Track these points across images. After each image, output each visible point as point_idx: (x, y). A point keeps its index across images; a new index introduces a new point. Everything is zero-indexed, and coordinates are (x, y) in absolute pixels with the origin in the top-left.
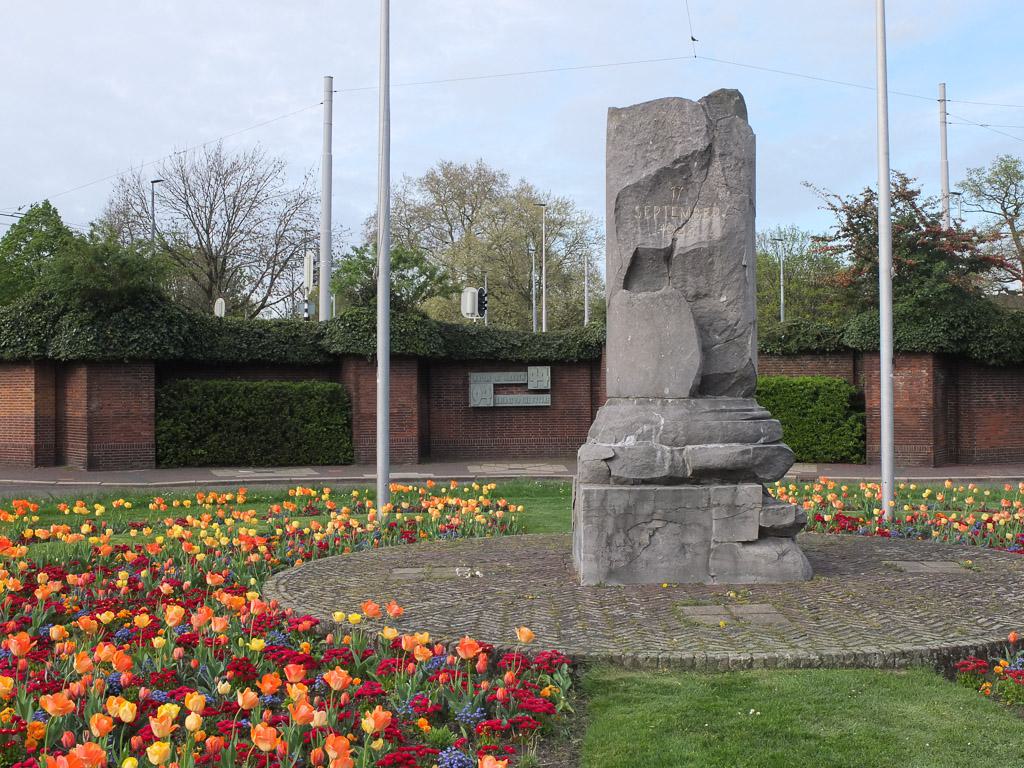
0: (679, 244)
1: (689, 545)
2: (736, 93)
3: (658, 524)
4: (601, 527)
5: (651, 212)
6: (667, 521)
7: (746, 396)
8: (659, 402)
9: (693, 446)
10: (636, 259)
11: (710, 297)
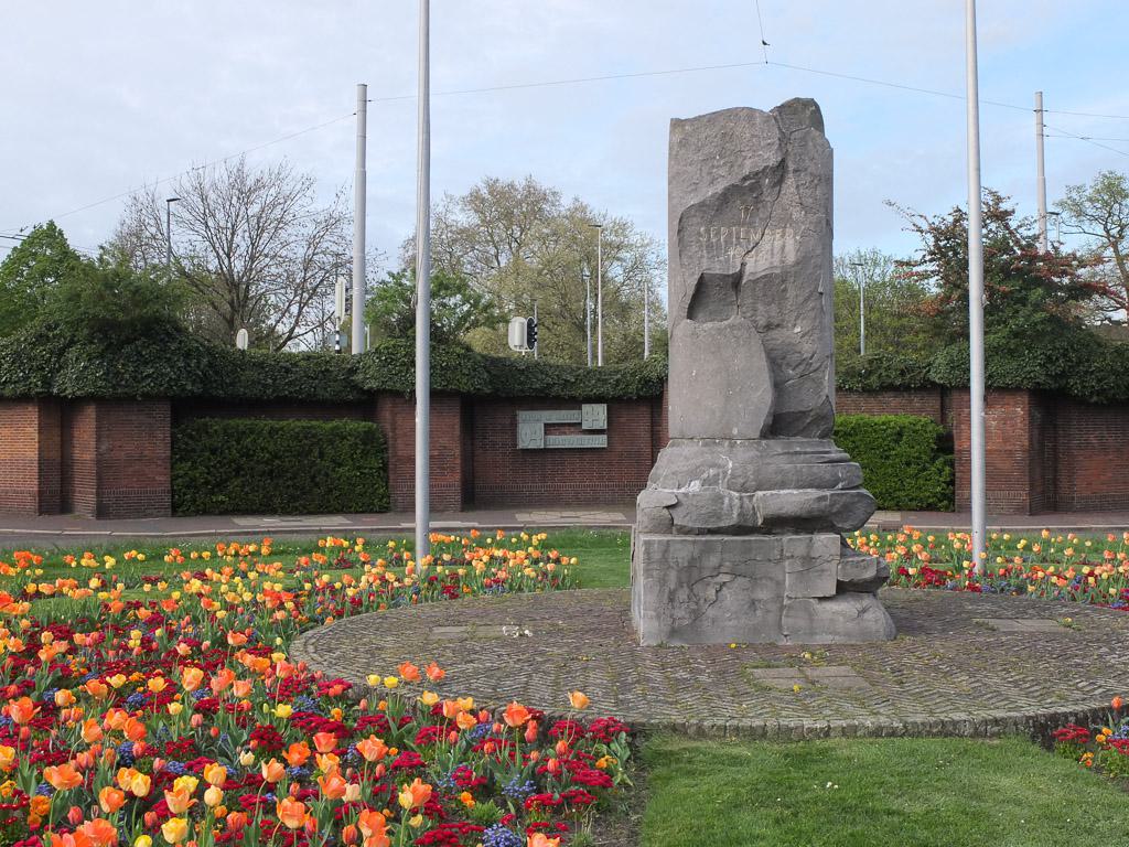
0: (748, 269)
1: (760, 601)
2: (812, 102)
3: (726, 578)
4: (663, 582)
5: (718, 233)
6: (735, 574)
7: (822, 436)
8: (727, 443)
9: (764, 492)
10: (702, 286)
11: (783, 328)
